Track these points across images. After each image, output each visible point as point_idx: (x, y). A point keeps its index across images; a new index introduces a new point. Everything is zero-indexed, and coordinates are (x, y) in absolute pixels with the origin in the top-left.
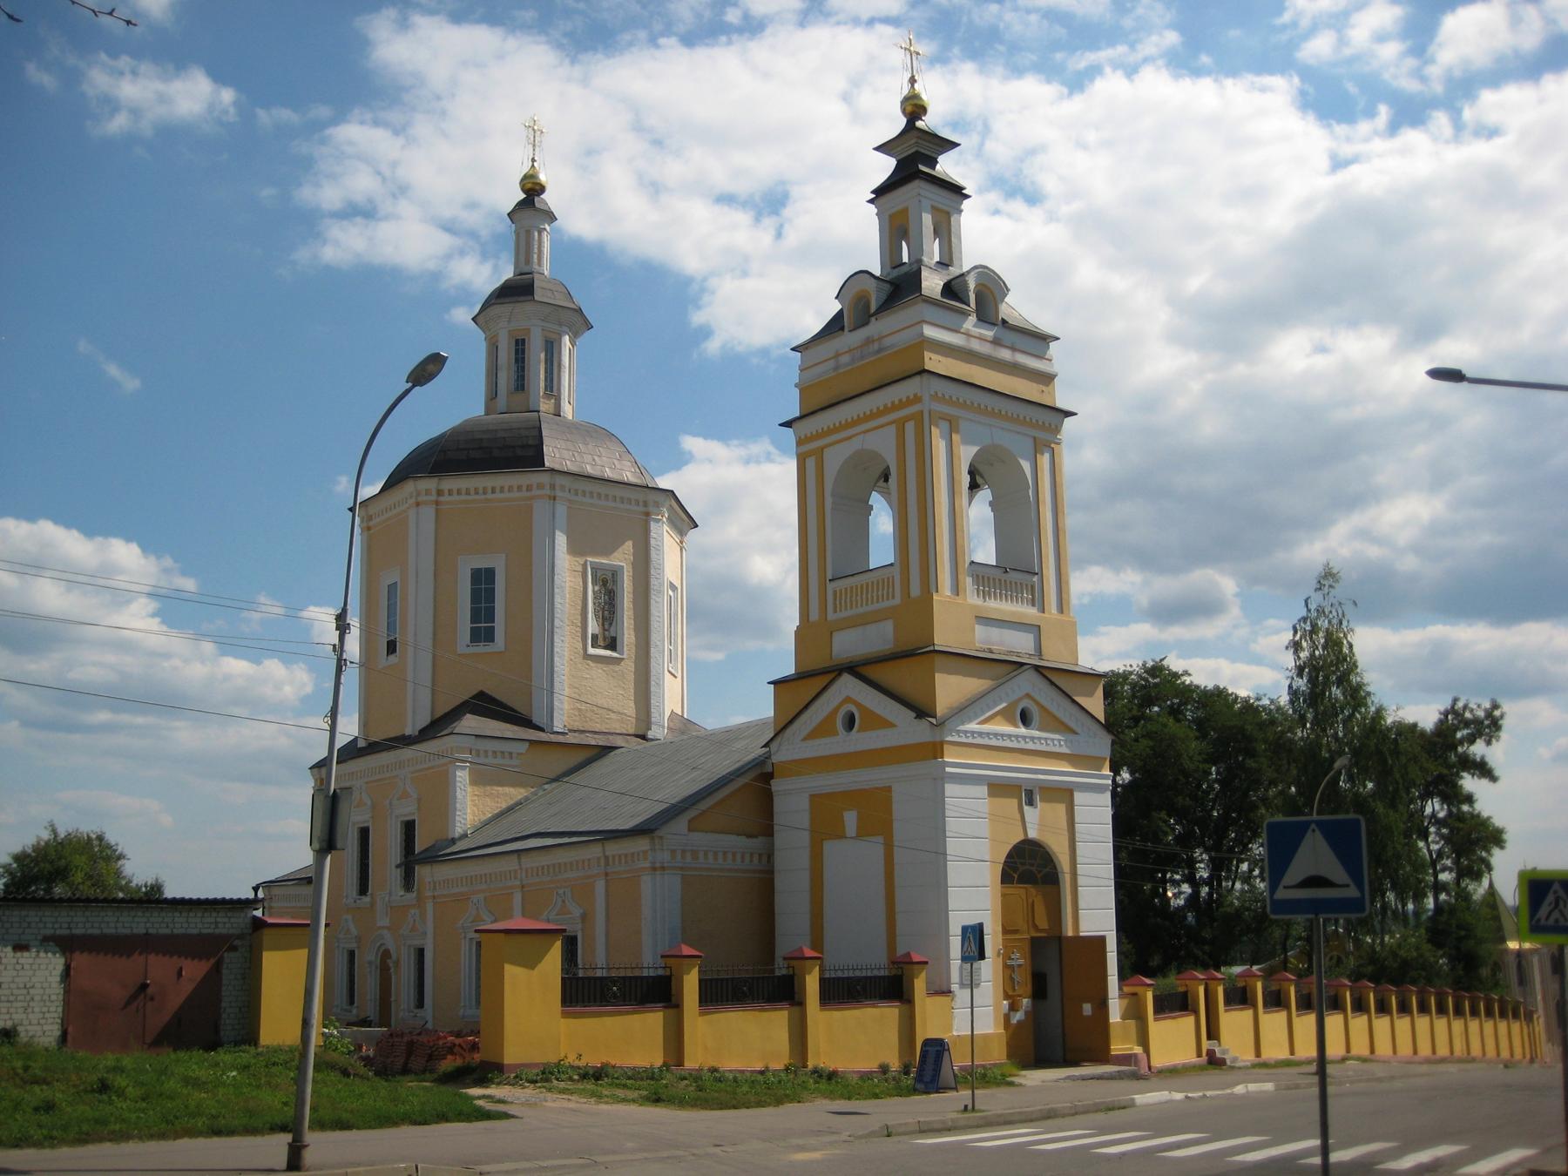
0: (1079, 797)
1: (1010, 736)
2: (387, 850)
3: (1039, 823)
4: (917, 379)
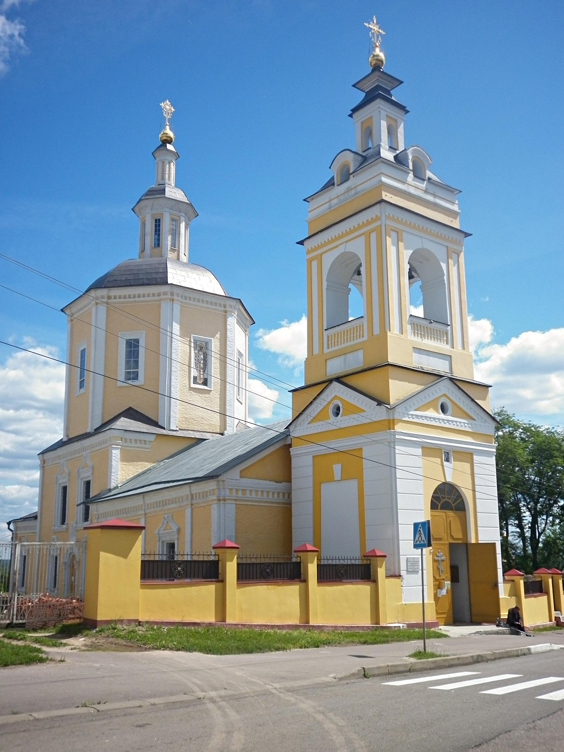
0: (475, 458)
1: (435, 419)
2: (76, 496)
3: (454, 473)
4: (377, 208)
